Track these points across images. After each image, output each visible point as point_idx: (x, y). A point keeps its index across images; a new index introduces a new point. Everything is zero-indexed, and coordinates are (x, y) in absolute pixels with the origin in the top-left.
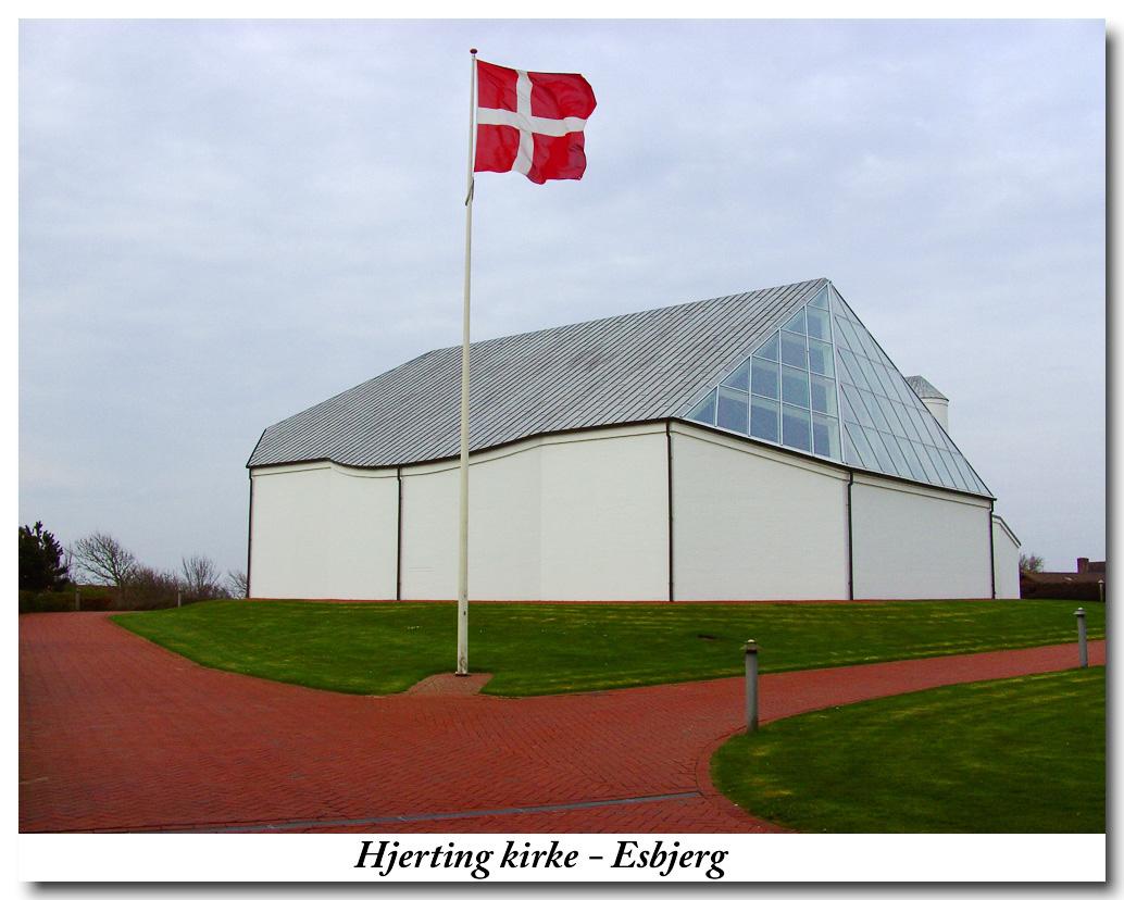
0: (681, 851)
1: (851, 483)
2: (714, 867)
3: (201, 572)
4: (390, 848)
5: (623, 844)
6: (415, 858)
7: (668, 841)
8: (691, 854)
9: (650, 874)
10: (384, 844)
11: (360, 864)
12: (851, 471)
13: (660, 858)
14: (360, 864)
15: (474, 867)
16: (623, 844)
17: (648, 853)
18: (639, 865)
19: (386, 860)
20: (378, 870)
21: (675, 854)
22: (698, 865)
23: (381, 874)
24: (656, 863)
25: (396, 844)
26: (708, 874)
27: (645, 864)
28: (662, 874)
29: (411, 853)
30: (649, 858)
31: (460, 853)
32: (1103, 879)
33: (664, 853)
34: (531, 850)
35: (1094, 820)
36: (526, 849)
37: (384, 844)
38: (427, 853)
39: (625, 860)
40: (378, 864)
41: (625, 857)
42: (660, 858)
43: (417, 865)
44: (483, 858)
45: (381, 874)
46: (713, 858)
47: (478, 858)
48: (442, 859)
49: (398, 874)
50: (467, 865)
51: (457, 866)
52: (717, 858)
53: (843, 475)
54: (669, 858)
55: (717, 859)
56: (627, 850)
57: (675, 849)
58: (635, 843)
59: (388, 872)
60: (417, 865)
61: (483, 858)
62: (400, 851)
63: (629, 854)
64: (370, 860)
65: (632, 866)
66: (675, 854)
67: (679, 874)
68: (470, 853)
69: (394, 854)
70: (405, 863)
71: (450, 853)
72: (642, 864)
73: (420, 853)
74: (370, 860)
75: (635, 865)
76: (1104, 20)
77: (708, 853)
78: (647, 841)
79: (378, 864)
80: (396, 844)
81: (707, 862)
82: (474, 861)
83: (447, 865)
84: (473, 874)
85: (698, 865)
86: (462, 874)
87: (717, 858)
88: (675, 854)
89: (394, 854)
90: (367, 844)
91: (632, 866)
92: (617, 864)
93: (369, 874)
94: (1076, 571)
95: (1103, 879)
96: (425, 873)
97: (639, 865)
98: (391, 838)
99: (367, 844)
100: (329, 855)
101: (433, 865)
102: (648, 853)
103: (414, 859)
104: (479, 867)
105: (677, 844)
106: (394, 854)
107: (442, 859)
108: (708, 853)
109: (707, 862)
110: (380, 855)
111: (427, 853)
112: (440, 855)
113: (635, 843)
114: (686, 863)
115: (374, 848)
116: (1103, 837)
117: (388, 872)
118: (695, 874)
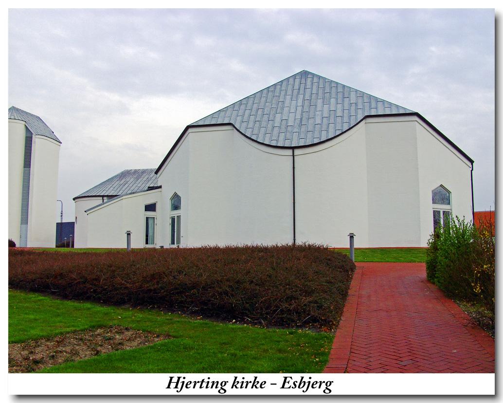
0: (312, 381)
2: (327, 388)
5: (286, 378)
7: (306, 377)
8: (191, 382)
9: (298, 391)
10: (179, 378)
11: (169, 387)
13: (303, 384)
14: (169, 387)
15: (219, 388)
16: (286, 378)
18: (293, 388)
20: (177, 389)
21: (309, 382)
22: (319, 388)
23: (177, 391)
24: (301, 387)
25: (184, 378)
26: (324, 391)
27: (296, 387)
28: (303, 391)
29: (317, 382)
30: (297, 384)
31: (213, 382)
32: (493, 393)
33: (304, 382)
34: (210, 381)
35: (490, 368)
36: (208, 380)
37: (179, 378)
38: (198, 382)
39: (287, 385)
40: (176, 387)
41: (286, 384)
42: (303, 384)
43: (194, 388)
44: (223, 384)
45: (177, 391)
46: (326, 384)
47: (221, 384)
48: (204, 385)
49: (185, 391)
50: (216, 387)
52: (328, 384)
53: (101, 198)
54: (307, 384)
56: (287, 381)
58: (291, 378)
60: (194, 388)
61: (223, 384)
62: (186, 381)
63: (288, 382)
64: (173, 385)
65: (290, 388)
66: (309, 382)
67: (311, 391)
68: (218, 382)
69: (183, 382)
70: (314, 386)
71: (208, 382)
72: (294, 387)
73: (321, 382)
74: (173, 385)
76: (494, 9)
77: (324, 382)
78: (297, 377)
79: (176, 387)
81: (324, 386)
82: (219, 386)
83: (207, 387)
85: (319, 388)
86: (214, 391)
87: (328, 384)
88: (309, 382)
89: (183, 382)
90: (171, 378)
91: (290, 388)
92: (283, 387)
93: (172, 391)
95: (493, 393)
97: (293, 388)
98: (182, 375)
99: (171, 378)
100: (155, 383)
101: (201, 387)
102: (297, 382)
103: (193, 384)
104: (222, 388)
105: (310, 378)
106: (183, 382)
107: (204, 385)
108: (324, 382)
109: (324, 386)
111: (198, 382)
112: (204, 383)
113: (291, 378)
114: (188, 386)
115: (175, 380)
116: (493, 375)
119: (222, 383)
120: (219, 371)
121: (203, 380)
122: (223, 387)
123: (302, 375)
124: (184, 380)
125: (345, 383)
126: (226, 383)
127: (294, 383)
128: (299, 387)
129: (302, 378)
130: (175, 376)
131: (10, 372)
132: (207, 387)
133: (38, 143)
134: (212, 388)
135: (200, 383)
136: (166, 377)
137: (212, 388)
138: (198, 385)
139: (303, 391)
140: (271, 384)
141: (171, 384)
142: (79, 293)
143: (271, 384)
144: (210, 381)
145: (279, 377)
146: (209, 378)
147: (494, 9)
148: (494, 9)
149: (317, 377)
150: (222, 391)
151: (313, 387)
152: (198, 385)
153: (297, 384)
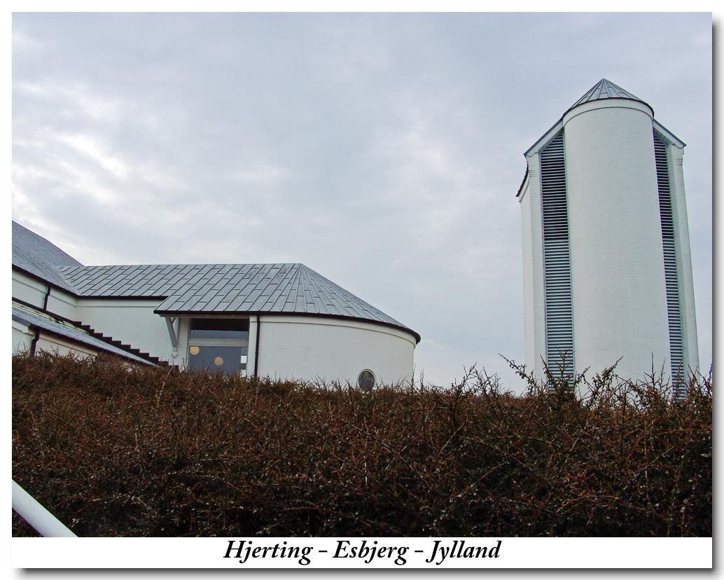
0: (378, 547)
1: (48, 294)
2: (399, 557)
3: (367, 378)
4: (246, 545)
5: (340, 543)
6: (262, 551)
7: (370, 542)
8: (260, 549)
9: (358, 563)
10: (242, 543)
11: (227, 556)
12: (50, 286)
13: (365, 551)
14: (227, 556)
15: (300, 558)
16: (340, 543)
17: (356, 548)
18: (350, 556)
19: (244, 553)
20: (239, 559)
21: (374, 549)
22: (389, 556)
23: (241, 562)
24: (362, 555)
25: (250, 543)
26: (396, 562)
27: (355, 555)
28: (366, 562)
29: (385, 549)
30: (357, 552)
31: (292, 548)
32: (710, 566)
33: (368, 549)
34: (288, 546)
35: (705, 529)
36: (284, 546)
37: (242, 543)
38: (270, 548)
39: (342, 553)
40: (238, 556)
41: (341, 551)
42: (365, 551)
43: (264, 556)
44: (306, 551)
45: (241, 562)
46: (399, 552)
47: (303, 552)
48: (279, 552)
49: (252, 563)
50: (296, 556)
51: (477, 556)
52: (402, 551)
53: (43, 289)
54: (371, 552)
55: (402, 552)
56: (343, 547)
57: (375, 546)
58: (348, 542)
59: (245, 560)
60: (264, 556)
61: (306, 551)
62: (253, 547)
63: (344, 549)
64: (233, 553)
65: (346, 556)
66: (374, 549)
67: (377, 563)
68: (298, 549)
69: (249, 549)
70: (382, 554)
71: (284, 549)
72: (352, 555)
73: (391, 548)
74: (233, 553)
75: (348, 556)
76: (710, 14)
77: (396, 548)
78: (356, 542)
79: (238, 556)
80: (250, 543)
81: (395, 554)
82: (300, 554)
83: (282, 556)
84: (300, 562)
85: (389, 556)
86: (292, 563)
87: (402, 551)
88: (375, 549)
89: (249, 549)
90: (231, 543)
91: (346, 556)
92: (337, 556)
93: (233, 563)
94: (242, 357)
95: (710, 566)
96: (279, 563)
97: (350, 556)
98: (247, 539)
99: (231, 543)
100: (207, 550)
101: (273, 556)
102: (356, 548)
103: (262, 552)
104: (304, 557)
105: (376, 543)
106: (249, 549)
107: (279, 552)
108: (396, 548)
109: (395, 554)
110: (240, 550)
111: (270, 548)
112: (278, 550)
113: (348, 542)
114: (256, 555)
115: (236, 545)
116: (710, 539)
117: (245, 560)
118: (387, 562)
119: (400, 549)
120: (300, 534)
121: (277, 546)
122: (305, 556)
123: (364, 539)
124: (250, 546)
125: (520, 551)
126: (309, 549)
127: (352, 550)
128: (360, 556)
129: (365, 542)
130: (237, 541)
131: (13, 536)
132: (282, 556)
133: (673, 152)
134: (477, 556)
135: (273, 550)
136: (224, 542)
137: (289, 556)
138: (270, 553)
139: (366, 562)
140: (416, 551)
141: (231, 551)
142: (133, 421)
143: (416, 551)
144: (288, 546)
145: (331, 543)
146: (285, 543)
147: (711, 13)
148: (711, 13)
149: (294, 542)
150: (304, 562)
151: (254, 556)
152: (270, 553)
153: (357, 552)
